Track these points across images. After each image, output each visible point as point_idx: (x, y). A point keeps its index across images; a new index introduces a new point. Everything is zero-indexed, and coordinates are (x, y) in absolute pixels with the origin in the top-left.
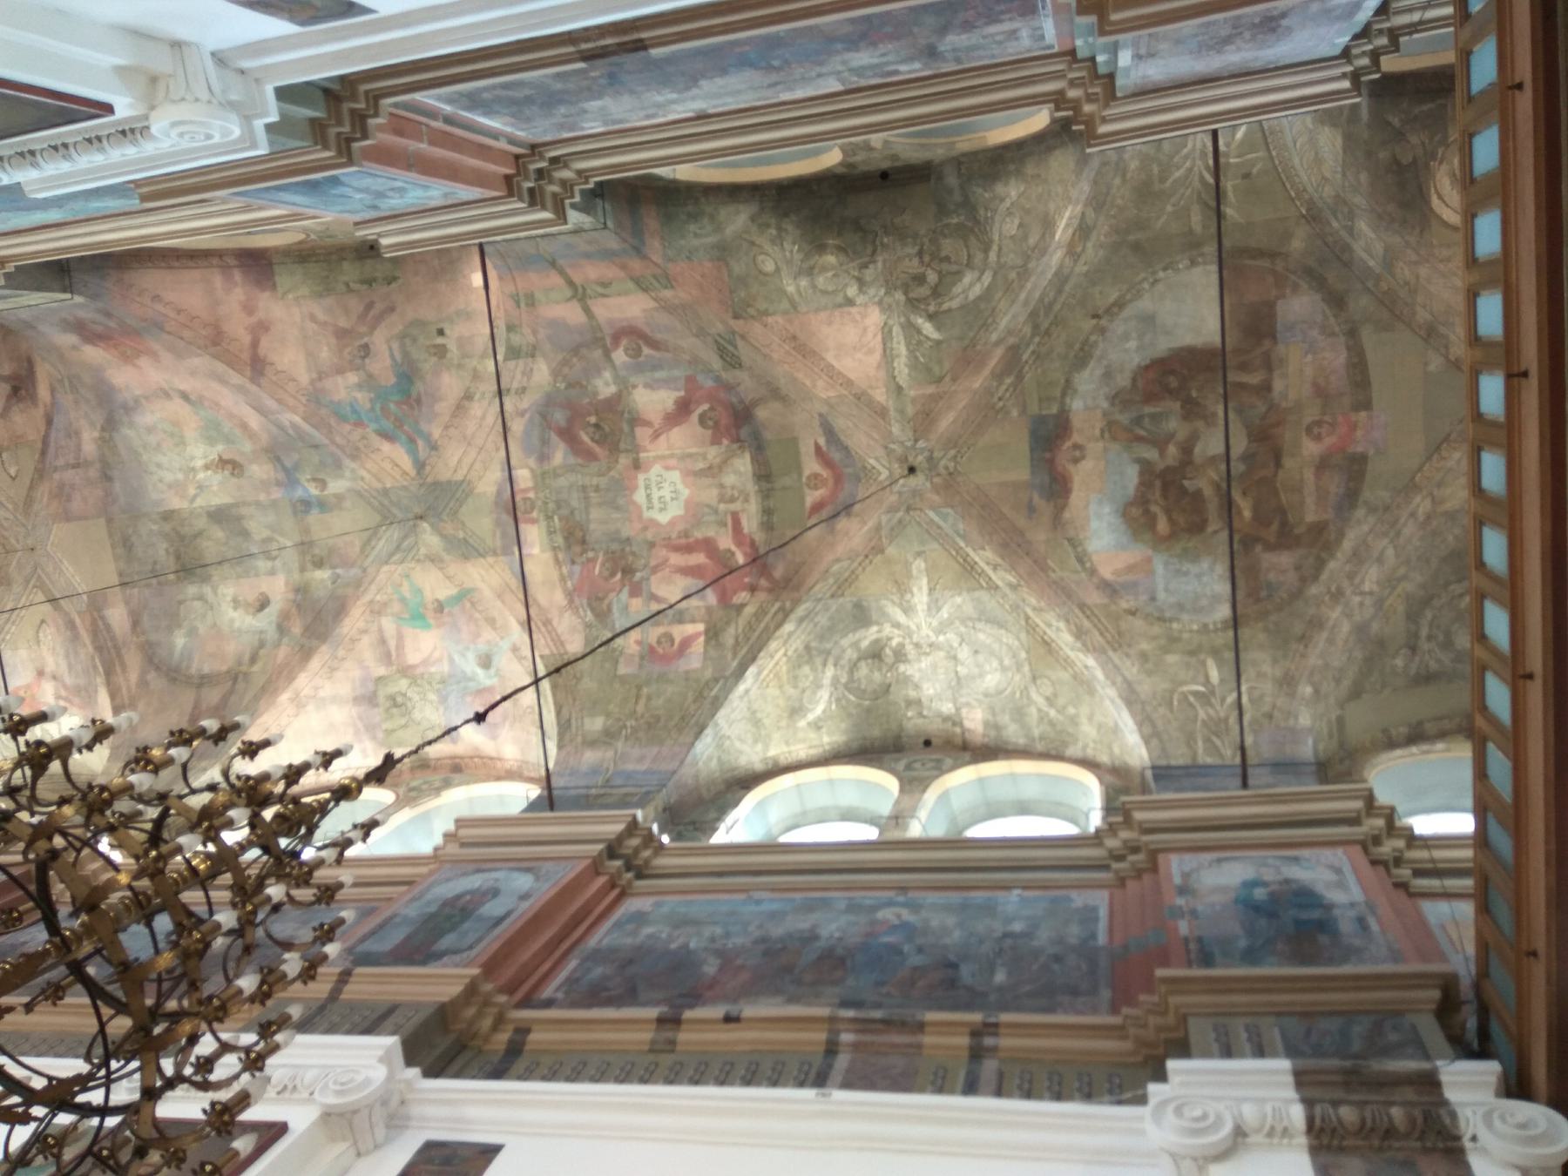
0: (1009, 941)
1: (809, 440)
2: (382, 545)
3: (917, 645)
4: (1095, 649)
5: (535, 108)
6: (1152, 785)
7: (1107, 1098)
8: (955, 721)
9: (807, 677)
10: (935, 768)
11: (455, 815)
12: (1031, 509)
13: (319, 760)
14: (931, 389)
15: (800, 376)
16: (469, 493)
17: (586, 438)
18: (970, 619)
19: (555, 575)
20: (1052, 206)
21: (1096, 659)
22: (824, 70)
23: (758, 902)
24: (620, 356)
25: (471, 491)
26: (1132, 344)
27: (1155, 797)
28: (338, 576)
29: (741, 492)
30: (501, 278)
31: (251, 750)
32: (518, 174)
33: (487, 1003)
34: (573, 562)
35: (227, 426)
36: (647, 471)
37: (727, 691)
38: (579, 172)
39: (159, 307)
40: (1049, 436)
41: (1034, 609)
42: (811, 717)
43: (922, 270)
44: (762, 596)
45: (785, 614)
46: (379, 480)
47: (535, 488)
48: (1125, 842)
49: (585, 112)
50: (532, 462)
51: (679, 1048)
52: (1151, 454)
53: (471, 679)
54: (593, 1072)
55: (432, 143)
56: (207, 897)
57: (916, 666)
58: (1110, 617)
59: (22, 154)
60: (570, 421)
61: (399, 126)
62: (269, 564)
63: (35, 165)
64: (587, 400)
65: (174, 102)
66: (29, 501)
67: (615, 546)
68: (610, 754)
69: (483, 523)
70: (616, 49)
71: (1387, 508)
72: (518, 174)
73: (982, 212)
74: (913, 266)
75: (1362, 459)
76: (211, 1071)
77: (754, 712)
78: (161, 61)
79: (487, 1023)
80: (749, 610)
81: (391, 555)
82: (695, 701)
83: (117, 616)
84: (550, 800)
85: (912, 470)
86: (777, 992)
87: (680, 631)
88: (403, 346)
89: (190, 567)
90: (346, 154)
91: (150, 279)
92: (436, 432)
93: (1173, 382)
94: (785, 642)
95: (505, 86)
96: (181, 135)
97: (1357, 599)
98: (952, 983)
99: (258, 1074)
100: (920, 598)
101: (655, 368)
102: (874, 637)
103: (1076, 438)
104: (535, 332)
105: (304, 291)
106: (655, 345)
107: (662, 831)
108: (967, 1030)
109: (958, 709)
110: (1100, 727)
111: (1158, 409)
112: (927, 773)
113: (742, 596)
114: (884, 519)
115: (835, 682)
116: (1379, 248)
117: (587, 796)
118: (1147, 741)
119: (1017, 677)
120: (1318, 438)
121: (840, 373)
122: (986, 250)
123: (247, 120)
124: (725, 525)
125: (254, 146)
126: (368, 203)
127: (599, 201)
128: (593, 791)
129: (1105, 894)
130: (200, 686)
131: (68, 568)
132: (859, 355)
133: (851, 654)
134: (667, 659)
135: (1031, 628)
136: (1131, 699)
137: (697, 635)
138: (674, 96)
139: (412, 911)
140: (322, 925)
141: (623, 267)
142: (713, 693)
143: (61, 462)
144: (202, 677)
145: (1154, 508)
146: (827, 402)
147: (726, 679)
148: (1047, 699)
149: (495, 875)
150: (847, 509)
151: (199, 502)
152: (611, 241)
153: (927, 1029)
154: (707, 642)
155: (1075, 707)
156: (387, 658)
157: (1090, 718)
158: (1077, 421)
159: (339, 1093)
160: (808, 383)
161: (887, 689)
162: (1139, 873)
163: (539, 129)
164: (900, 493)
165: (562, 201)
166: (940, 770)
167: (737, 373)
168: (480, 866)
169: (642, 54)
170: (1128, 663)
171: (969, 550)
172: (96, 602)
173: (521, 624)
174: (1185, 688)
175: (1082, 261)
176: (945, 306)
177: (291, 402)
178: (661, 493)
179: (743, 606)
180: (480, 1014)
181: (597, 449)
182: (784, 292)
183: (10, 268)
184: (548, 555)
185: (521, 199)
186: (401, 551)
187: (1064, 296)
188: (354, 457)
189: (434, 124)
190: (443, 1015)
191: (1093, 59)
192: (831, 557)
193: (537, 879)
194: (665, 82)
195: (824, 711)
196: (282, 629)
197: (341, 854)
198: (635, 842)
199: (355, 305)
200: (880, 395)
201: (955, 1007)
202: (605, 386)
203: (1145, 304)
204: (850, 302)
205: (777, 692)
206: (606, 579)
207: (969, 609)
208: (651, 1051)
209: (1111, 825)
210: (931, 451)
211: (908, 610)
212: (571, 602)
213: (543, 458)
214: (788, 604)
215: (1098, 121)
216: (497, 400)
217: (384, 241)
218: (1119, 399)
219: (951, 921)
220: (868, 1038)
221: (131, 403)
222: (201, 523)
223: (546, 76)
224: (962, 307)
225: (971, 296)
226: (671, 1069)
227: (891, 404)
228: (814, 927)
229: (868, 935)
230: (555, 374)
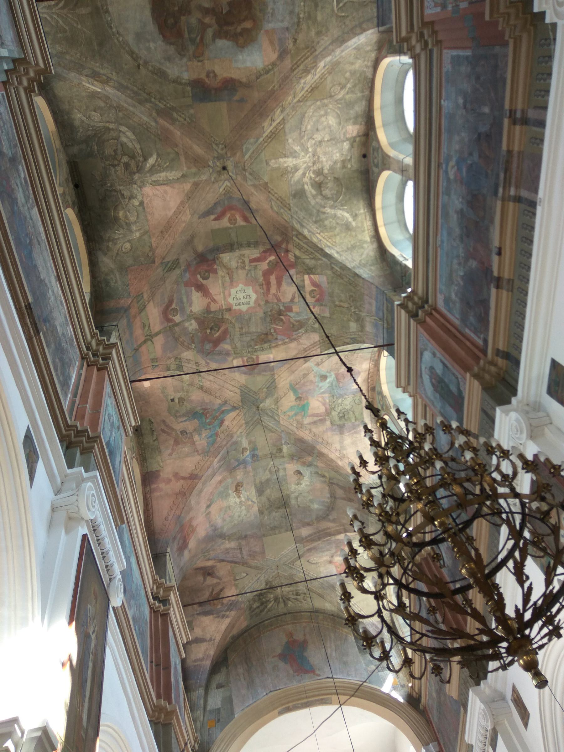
0: (468, 106)
1: (212, 224)
2: (271, 424)
3: (314, 163)
4: (315, 62)
5: (65, 357)
6: (388, 26)
7: (552, 47)
9: (330, 222)
10: (377, 151)
11: (395, 388)
13: (368, 434)
14: (183, 159)
15: (180, 229)
16: (246, 387)
17: (218, 334)
18: (300, 134)
19: (282, 347)
20: (84, 94)
21: (320, 61)
22: (29, 217)
23: (442, 242)
24: (177, 319)
25: (245, 386)
26: (152, 45)
27: (394, 25)
28: (286, 442)
29: (240, 258)
30: (145, 374)
31: (364, 463)
32: (96, 365)
33: (483, 369)
34: (276, 339)
35: (221, 489)
36: (231, 305)
37: (337, 262)
38: (92, 337)
39: (170, 518)
40: (204, 91)
41: (294, 97)
42: (350, 219)
43: (122, 165)
44: (290, 246)
45: (300, 234)
46: (242, 426)
47: (242, 357)
48: (418, 41)
49: (63, 334)
50: (230, 359)
51: (512, 277)
52: (210, 32)
53: (332, 384)
54: (520, 318)
55: (87, 403)
56: (429, 477)
57: (325, 163)
58: (297, 53)
59: (108, 571)
60: (210, 341)
61: (80, 416)
62: (281, 471)
63: (112, 565)
64: (199, 334)
65: (79, 509)
66: (256, 568)
67: (268, 319)
68: (368, 319)
69: (259, 381)
70: (31, 318)
72: (96, 365)
73: (90, 133)
74: (120, 169)
76: (508, 475)
77: (348, 249)
78: (61, 516)
79: (493, 369)
80: (297, 253)
82: (342, 279)
83: (305, 532)
84: (389, 346)
85: (224, 168)
86: (487, 229)
87: (308, 287)
88: (180, 417)
89: (283, 503)
90: (96, 438)
91: (158, 522)
92: (219, 402)
93: (171, 21)
94: (313, 233)
95: (56, 370)
96: (93, 507)
98: (488, 136)
99: (511, 453)
100: (290, 162)
101: (182, 302)
102: (310, 187)
103: (203, 76)
104: (169, 358)
105: (159, 458)
106: (170, 302)
107: (406, 292)
108: (512, 127)
109: (347, 139)
110: (357, 58)
111: (186, 30)
112: (380, 155)
113: (291, 257)
114: (250, 183)
115: (332, 207)
117: (387, 329)
118: (364, 30)
119: (331, 106)
121: (177, 208)
122: (109, 129)
123: (84, 480)
125: (95, 477)
126: (116, 431)
127: (105, 329)
128: (385, 326)
129: (445, 51)
130: (335, 498)
131: (285, 552)
132: (168, 199)
133: (319, 199)
134: (322, 293)
135: (304, 99)
136: (341, 40)
137: (311, 279)
138: (50, 291)
139: (439, 405)
140: (443, 430)
141: (135, 317)
142: (339, 270)
143: (239, 555)
144: (331, 497)
145: (239, 30)
146: (192, 215)
147: (331, 263)
148: (341, 89)
149: (423, 368)
150: (246, 203)
151: (255, 500)
152: (123, 323)
153: (511, 149)
155: (346, 72)
156: (322, 421)
157: (352, 64)
158: (195, 76)
159: (521, 432)
160: (183, 225)
161: (337, 179)
162: (434, 33)
163: (74, 355)
164: (236, 175)
165: (106, 345)
166: (379, 148)
168: (419, 376)
169: (32, 305)
170: (322, 42)
171: (265, 135)
172: (298, 540)
173: (306, 362)
174: (335, 9)
175: (110, 75)
176: (140, 152)
177: (208, 463)
178: (242, 298)
179: (295, 256)
180: (489, 372)
181: (222, 329)
183: (157, 577)
184: (273, 351)
185: (108, 364)
186: (273, 416)
187: (129, 85)
188: (232, 437)
189: (77, 402)
190: (487, 388)
191: (6, 71)
193: (426, 349)
194: (44, 295)
195: (348, 213)
196: (310, 465)
197: (411, 422)
198: (410, 304)
199: (163, 437)
200: (187, 186)
201: (501, 134)
202: (192, 326)
203: (130, 39)
204: (142, 203)
205: (338, 237)
206: (284, 323)
207: (295, 135)
208: (512, 291)
209: (408, 50)
210: (214, 158)
212: (295, 339)
213: (228, 354)
214: (294, 233)
215: (38, 68)
216: (202, 374)
217: (133, 424)
218: (181, 51)
219: (456, 138)
220: (513, 180)
221: (213, 528)
222: (264, 499)
223: (49, 351)
224: (139, 142)
225: (133, 137)
226: (522, 281)
227: (192, 180)
228: (457, 212)
229: (462, 183)
230: (188, 348)
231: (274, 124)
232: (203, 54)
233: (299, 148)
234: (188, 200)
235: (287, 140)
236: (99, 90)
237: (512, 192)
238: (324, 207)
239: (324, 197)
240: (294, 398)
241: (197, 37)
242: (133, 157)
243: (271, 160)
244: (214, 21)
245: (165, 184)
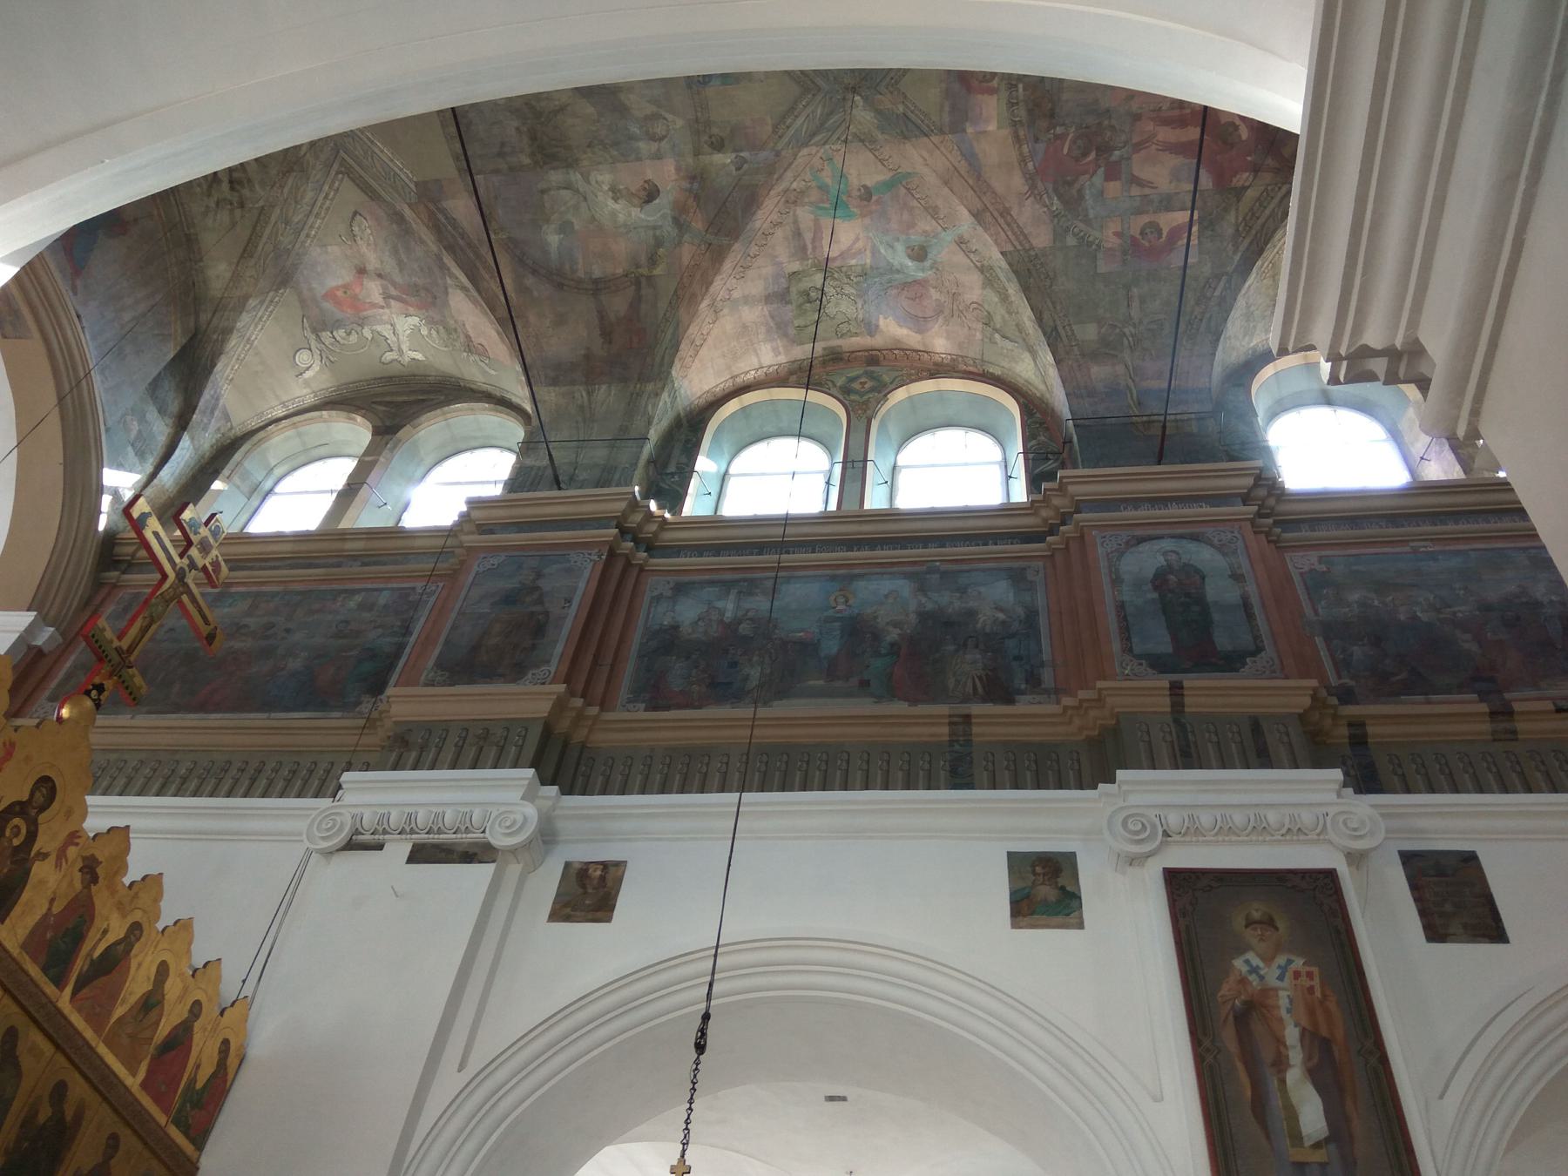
28: (745, 161)
44: (1267, 177)
53: (898, 271)
62: (654, 146)
68: (1120, 369)
81: (813, 135)
83: (461, 207)
113: (1244, 178)
144: (596, 281)
156: (801, 251)
184: (1006, 132)
206: (1077, 160)
212: (1033, 187)
240: (868, 184)
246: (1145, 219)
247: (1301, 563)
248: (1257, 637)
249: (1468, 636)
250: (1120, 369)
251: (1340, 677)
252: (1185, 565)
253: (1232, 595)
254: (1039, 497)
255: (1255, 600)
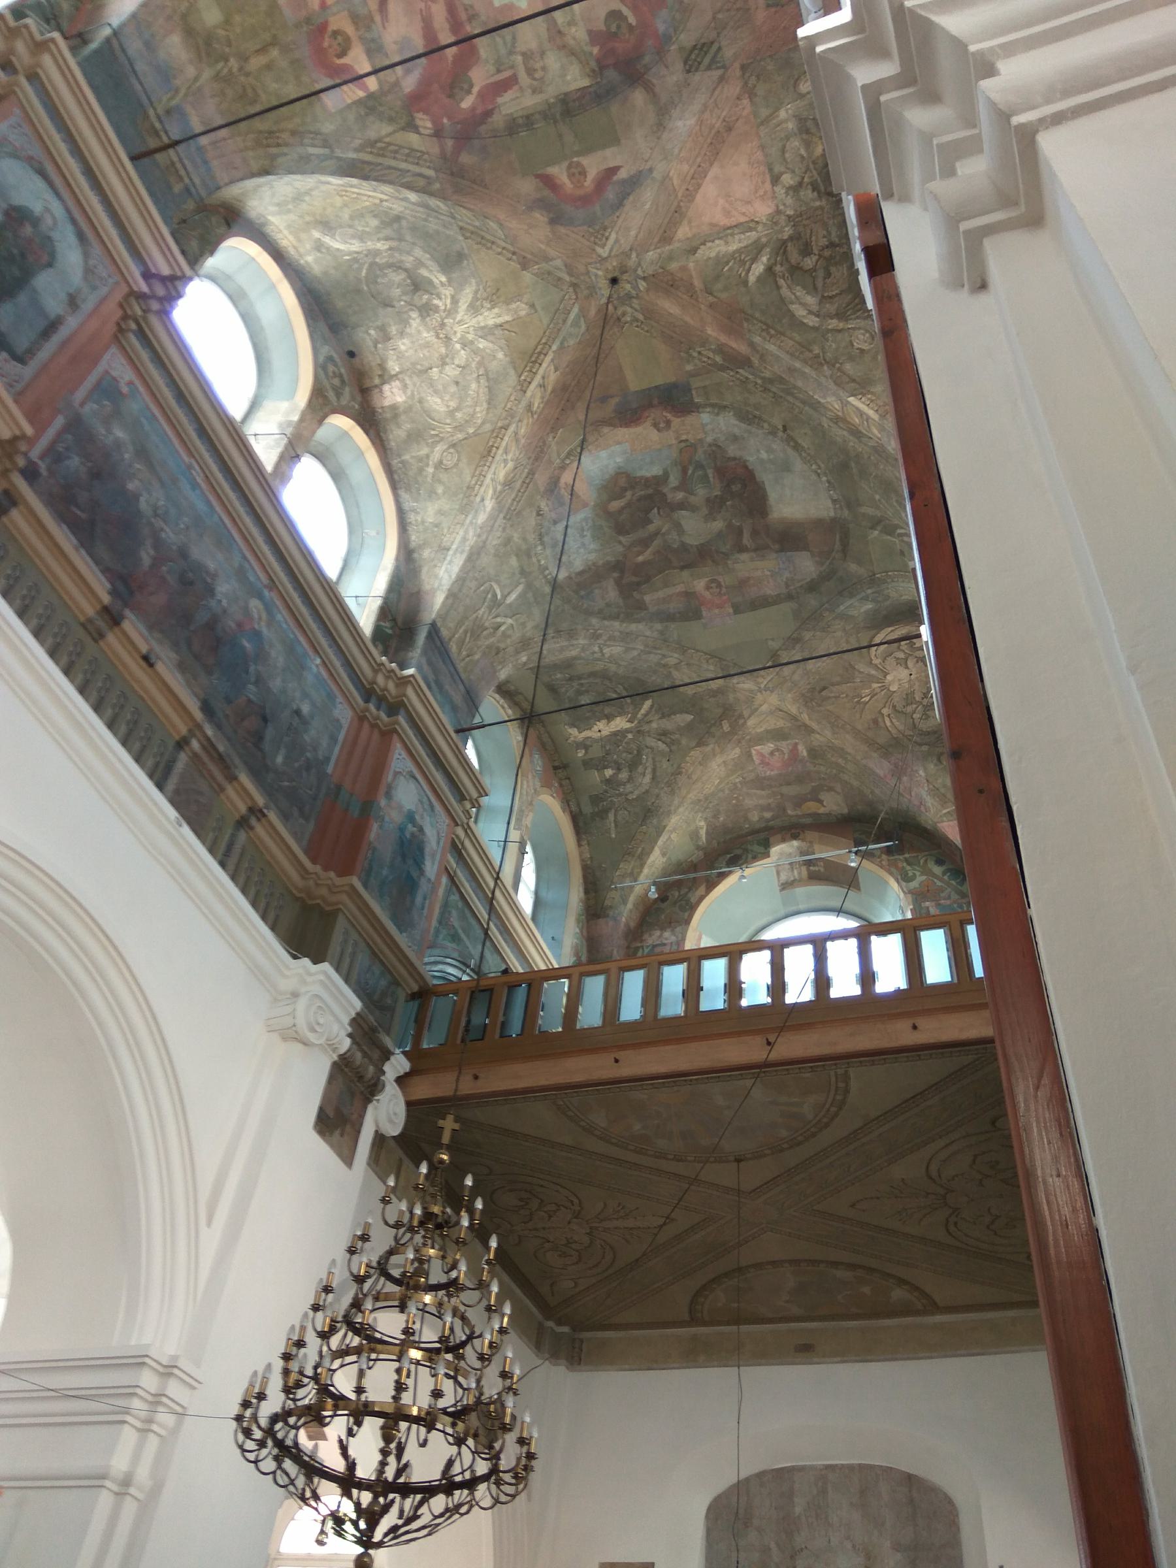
3: (443, 325)
4: (499, 503)
8: (386, 377)
12: (604, 399)
14: (698, 284)
21: (493, 509)
40: (673, 399)
41: (516, 434)
42: (327, 240)
51: (101, 643)
52: (674, 481)
68: (191, 71)
71: (665, 641)
75: (697, 615)
94: (397, 198)
97: (596, 649)
102: (435, 280)
103: (676, 422)
108: (250, 804)
109: (395, 377)
113: (425, 122)
115: (377, 253)
116: (855, 613)
120: (708, 588)
121: (699, 186)
124: (499, 71)
133: (408, 261)
142: (311, 150)
145: (629, 494)
148: (441, 462)
150: (556, 220)
154: (359, 102)
155: (444, 493)
158: (691, 419)
161: (387, 304)
167: (679, 66)
174: (495, 586)
176: (781, 282)
182: (777, 109)
187: (801, 406)
192: (502, 217)
200: (683, 232)
203: (798, 465)
204: (775, 180)
207: (494, 366)
208: (83, 625)
211: (474, 309)
214: (437, 186)
218: (716, 450)
220: (206, 759)
224: (782, 300)
225: (793, 307)
231: (538, 379)
232: (681, 451)
233: (481, 346)
234: (679, 206)
235: (506, 355)
236: (851, 399)
237: (195, 744)
238: (391, 249)
239: (400, 268)
241: (693, 473)
242: (795, 270)
243: (528, 315)
244: (670, 496)
245: (729, 228)
246: (350, 30)
247: (115, 365)
248: (31, 352)
249: (152, 552)
250: (191, 71)
251: (42, 457)
252: (49, 238)
253: (54, 305)
254: (12, 23)
255: (63, 332)
